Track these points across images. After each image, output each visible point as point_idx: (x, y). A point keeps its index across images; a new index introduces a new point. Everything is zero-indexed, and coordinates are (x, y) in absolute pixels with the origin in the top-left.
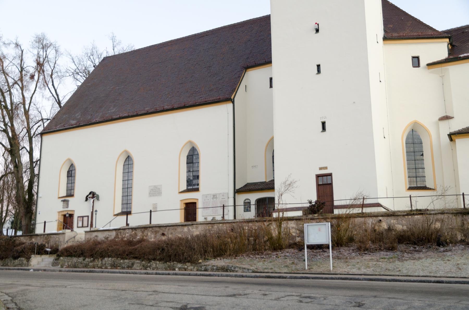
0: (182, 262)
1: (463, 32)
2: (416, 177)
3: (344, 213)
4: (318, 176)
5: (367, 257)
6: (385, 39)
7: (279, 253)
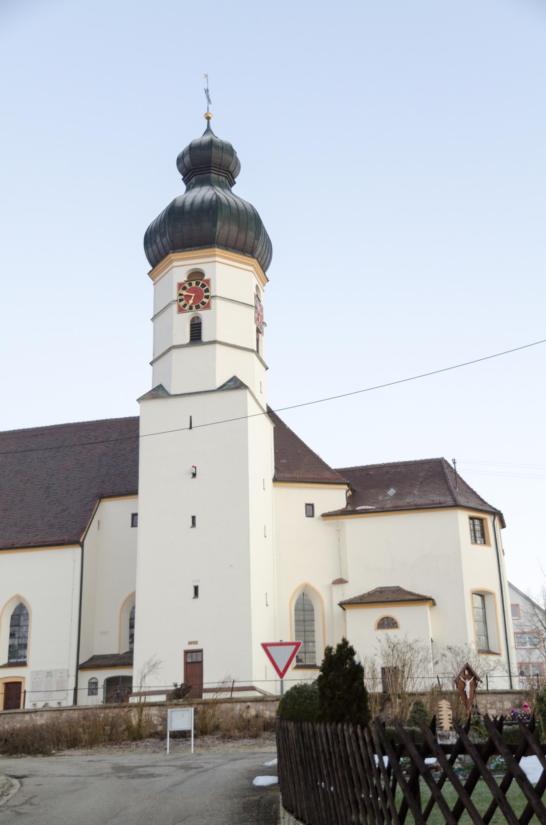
0: (32, 753)
1: (367, 474)
2: (305, 653)
3: (211, 698)
4: (186, 652)
5: (230, 745)
6: (275, 480)
7: (139, 743)
